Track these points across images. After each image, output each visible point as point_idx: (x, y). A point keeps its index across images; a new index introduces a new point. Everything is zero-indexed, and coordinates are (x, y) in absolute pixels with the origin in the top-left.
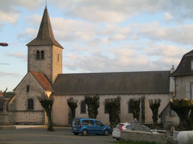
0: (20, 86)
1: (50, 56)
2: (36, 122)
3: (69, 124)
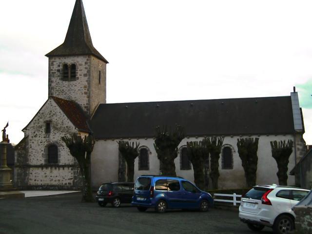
1: (86, 73)
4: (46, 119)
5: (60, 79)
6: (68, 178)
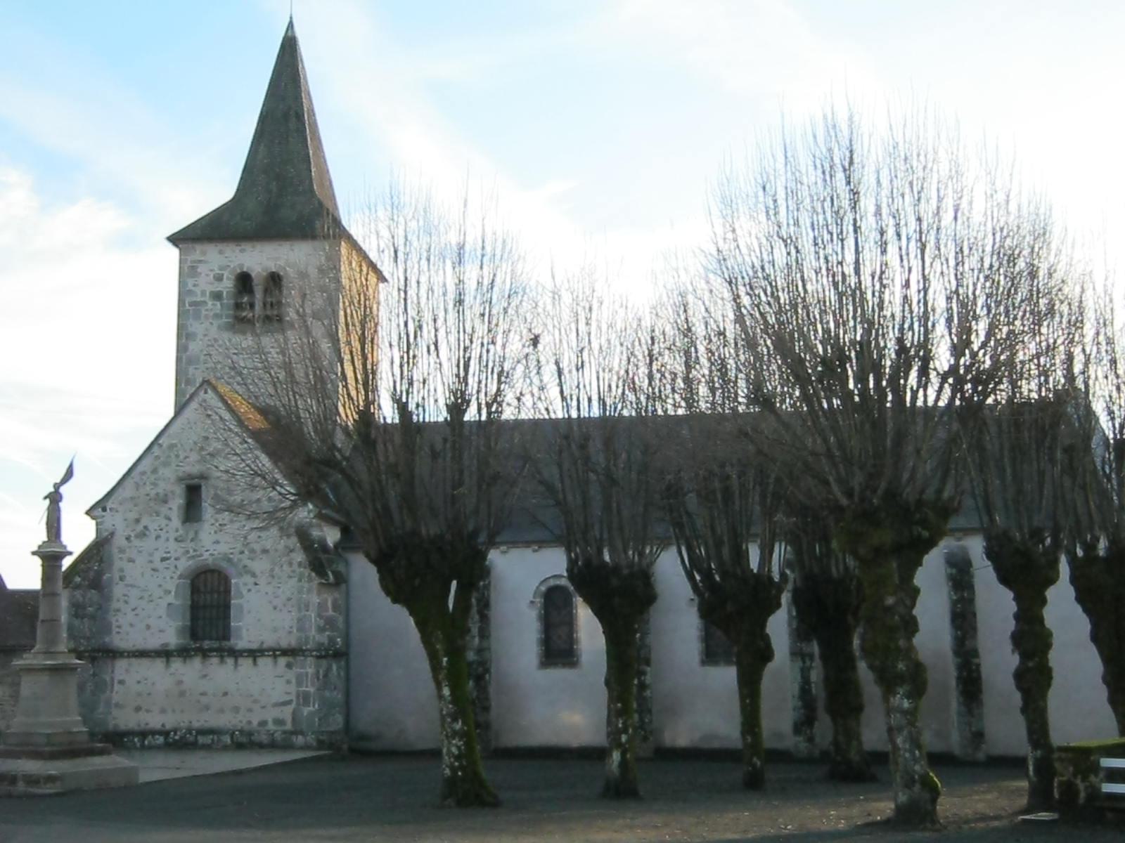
0: (137, 486)
2: (247, 728)
5: (219, 327)
6: (274, 701)
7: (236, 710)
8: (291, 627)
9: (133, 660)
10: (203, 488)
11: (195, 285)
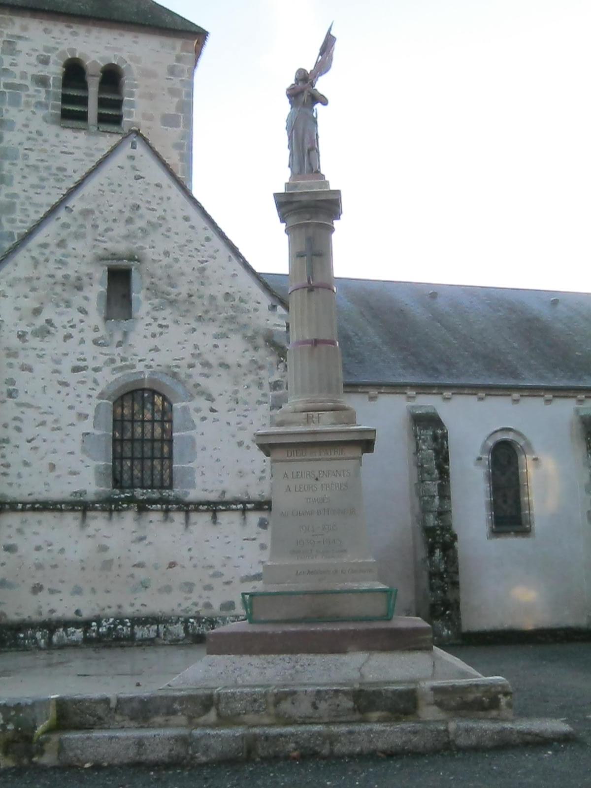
0: (36, 263)
1: (172, 111)
2: (204, 613)
3: (439, 623)
4: (109, 245)
7: (189, 587)
8: (263, 471)
9: (29, 515)
10: (134, 275)
11: (12, 64)
